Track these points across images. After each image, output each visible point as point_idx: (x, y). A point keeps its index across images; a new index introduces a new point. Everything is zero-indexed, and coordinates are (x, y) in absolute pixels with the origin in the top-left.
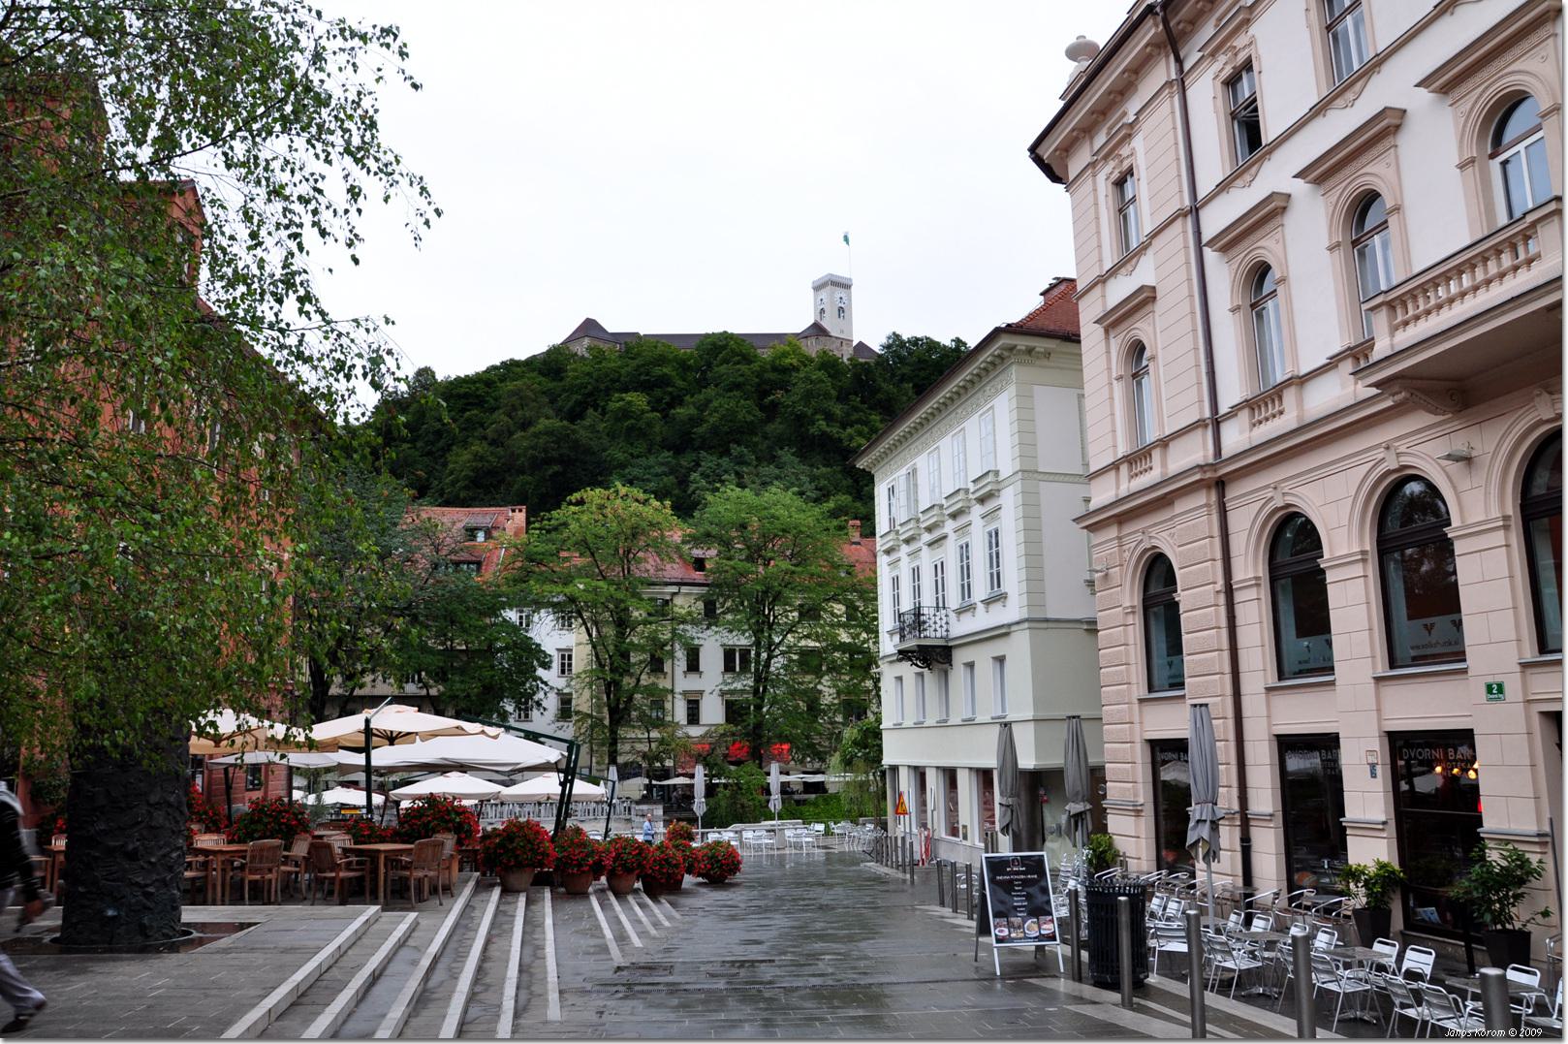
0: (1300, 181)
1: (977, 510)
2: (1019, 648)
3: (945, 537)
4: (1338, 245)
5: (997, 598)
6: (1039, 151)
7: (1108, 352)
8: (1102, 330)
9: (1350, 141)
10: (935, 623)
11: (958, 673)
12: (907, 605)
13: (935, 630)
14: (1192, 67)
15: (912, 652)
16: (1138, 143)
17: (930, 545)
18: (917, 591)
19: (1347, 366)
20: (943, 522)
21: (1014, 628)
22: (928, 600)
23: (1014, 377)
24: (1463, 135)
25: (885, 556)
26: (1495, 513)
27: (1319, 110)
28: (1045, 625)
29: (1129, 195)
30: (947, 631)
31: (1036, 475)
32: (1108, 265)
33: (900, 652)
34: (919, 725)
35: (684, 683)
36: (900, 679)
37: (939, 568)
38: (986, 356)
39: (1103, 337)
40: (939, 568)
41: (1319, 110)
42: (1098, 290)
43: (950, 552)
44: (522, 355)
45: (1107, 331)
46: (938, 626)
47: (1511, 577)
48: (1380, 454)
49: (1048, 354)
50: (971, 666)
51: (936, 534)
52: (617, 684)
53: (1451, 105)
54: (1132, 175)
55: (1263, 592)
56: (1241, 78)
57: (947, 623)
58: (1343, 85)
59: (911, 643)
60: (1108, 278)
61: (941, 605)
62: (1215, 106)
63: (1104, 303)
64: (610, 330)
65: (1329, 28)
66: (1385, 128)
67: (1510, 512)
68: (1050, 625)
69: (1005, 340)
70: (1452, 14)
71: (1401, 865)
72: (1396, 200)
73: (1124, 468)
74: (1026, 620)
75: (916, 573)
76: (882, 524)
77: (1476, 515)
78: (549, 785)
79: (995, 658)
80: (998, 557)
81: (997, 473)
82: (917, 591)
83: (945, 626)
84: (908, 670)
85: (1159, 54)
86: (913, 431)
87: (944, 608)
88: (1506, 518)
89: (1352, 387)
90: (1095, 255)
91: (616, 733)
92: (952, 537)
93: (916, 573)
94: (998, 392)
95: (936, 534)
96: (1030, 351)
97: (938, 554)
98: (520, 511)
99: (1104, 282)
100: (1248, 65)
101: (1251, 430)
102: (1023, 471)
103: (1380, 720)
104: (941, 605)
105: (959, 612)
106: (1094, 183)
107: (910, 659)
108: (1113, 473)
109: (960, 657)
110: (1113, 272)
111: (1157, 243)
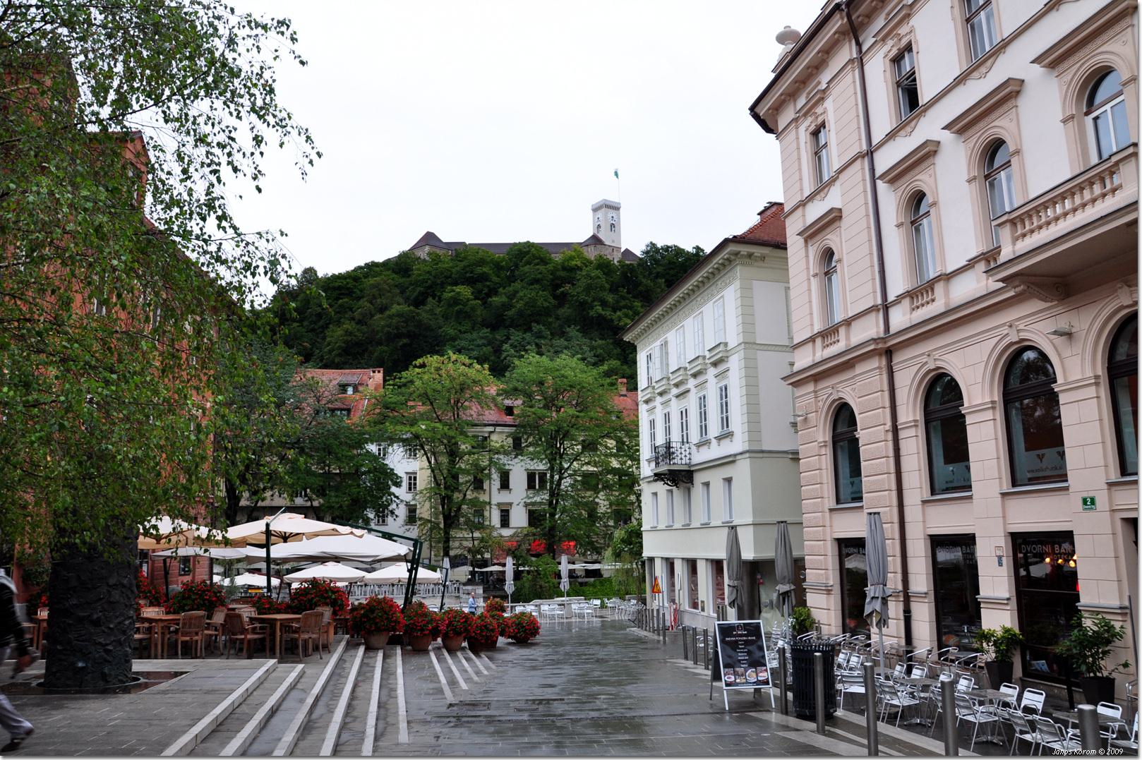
0: (947, 132)
1: (712, 372)
2: (742, 472)
3: (688, 391)
4: (975, 178)
5: (726, 436)
6: (757, 110)
7: (807, 256)
8: (803, 240)
9: (983, 103)
10: (681, 453)
11: (698, 490)
12: (660, 441)
13: (681, 459)
14: (868, 49)
15: (665, 475)
16: (829, 104)
17: (678, 396)
18: (668, 430)
19: (981, 267)
20: (687, 380)
21: (738, 457)
22: (676, 437)
23: (738, 274)
24: (1065, 98)
25: (645, 405)
26: (1089, 373)
27: (960, 80)
28: (761, 455)
29: (822, 142)
30: (690, 459)
31: (754, 346)
32: (807, 193)
33: (656, 475)
34: (669, 528)
35: (498, 497)
36: (655, 494)
37: (684, 414)
38: (718, 259)
39: (804, 245)
40: (684, 414)
41: (960, 80)
42: (800, 211)
43: (692, 402)
44: (380, 259)
45: (806, 241)
46: (683, 456)
47: (1101, 420)
48: (1005, 330)
49: (763, 258)
50: (707, 484)
51: (682, 389)
52: (449, 498)
53: (1057, 77)
54: (825, 127)
55: (920, 431)
56: (904, 57)
57: (690, 454)
58: (978, 62)
59: (664, 468)
60: (807, 202)
61: (685, 440)
62: (885, 77)
63: (804, 221)
64: (444, 240)
65: (968, 20)
66: (1009, 93)
67: (1100, 373)
68: (765, 455)
69: (732, 248)
70: (1058, 10)
71: (1020, 630)
72: (1016, 145)
73: (819, 341)
74: (748, 452)
75: (667, 417)
76: (642, 382)
77: (1075, 375)
78: (400, 571)
79: (725, 479)
80: (727, 405)
81: (726, 344)
82: (668, 430)
83: (688, 456)
84: (661, 488)
85: (844, 39)
86: (665, 314)
87: (688, 442)
88: (1097, 377)
89: (985, 282)
90: (797, 186)
91: (448, 534)
92: (693, 391)
93: (667, 417)
94: (727, 285)
95: (682, 389)
96: (750, 256)
97: (683, 403)
98: (379, 372)
99: (804, 205)
100: (909, 48)
101: (911, 313)
102: (745, 343)
103: (1005, 524)
104: (685, 440)
105: (699, 445)
106: (797, 133)
107: (662, 480)
108: (811, 344)
109: (699, 478)
110: (811, 198)
111: (843, 177)
